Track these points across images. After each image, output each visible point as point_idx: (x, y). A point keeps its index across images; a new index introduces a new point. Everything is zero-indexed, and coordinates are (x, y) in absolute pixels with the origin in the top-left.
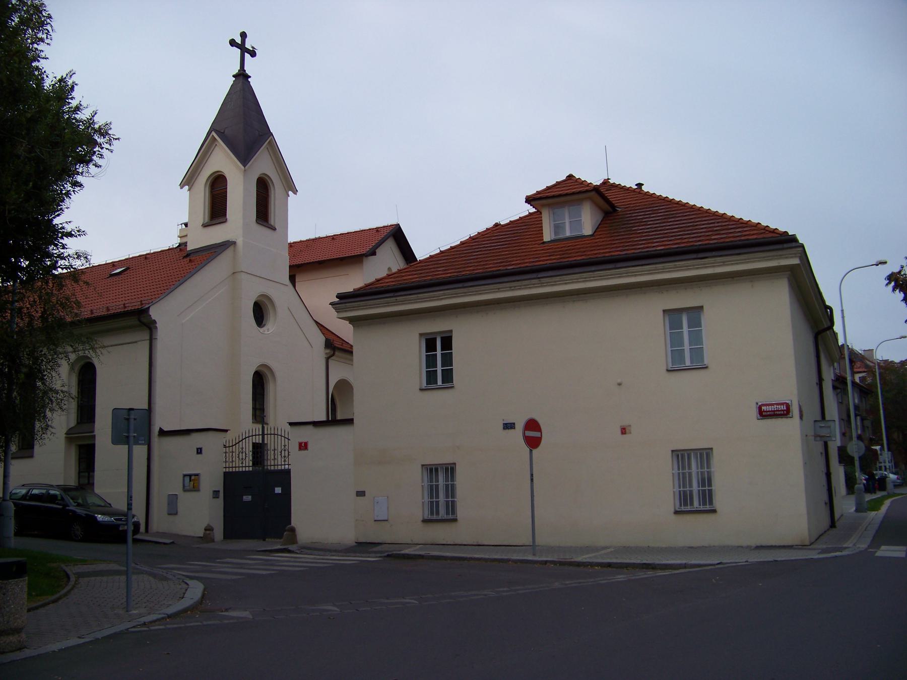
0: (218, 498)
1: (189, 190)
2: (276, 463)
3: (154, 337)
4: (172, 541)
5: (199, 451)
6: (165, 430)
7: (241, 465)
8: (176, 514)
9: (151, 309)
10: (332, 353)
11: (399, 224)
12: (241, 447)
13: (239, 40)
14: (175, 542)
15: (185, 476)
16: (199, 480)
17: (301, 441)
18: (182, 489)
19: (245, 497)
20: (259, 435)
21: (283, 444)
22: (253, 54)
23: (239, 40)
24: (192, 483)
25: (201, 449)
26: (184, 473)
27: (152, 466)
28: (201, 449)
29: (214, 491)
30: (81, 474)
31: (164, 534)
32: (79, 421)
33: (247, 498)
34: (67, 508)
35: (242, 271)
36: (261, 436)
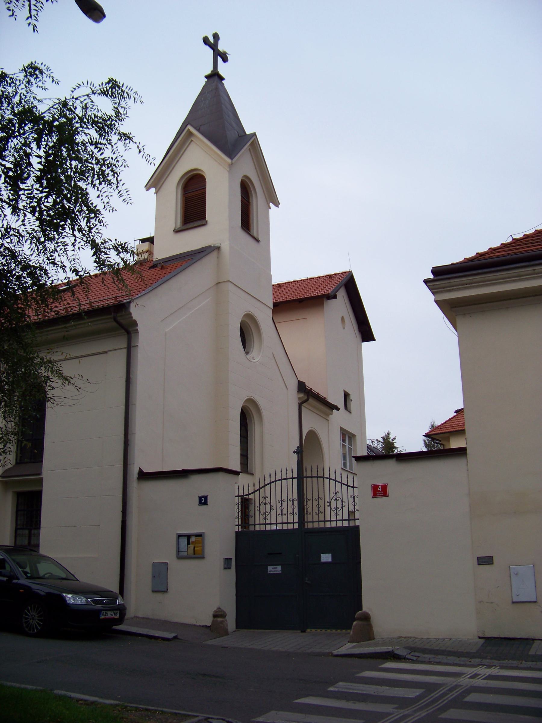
0: (230, 568)
1: (156, 192)
2: (322, 519)
3: (133, 344)
4: (173, 635)
5: (203, 501)
6: (145, 472)
7: (334, 518)
8: (166, 591)
9: (132, 305)
10: (306, 398)
11: (351, 271)
12: (262, 494)
13: (212, 40)
14: (178, 637)
15: (180, 536)
16: (203, 543)
17: (376, 483)
18: (175, 556)
19: (270, 568)
20: (306, 477)
21: (333, 490)
22: (225, 60)
23: (212, 40)
24: (192, 546)
25: (206, 498)
26: (178, 532)
27: (128, 523)
28: (206, 498)
29: (226, 559)
30: (19, 532)
31: (147, 621)
32: (18, 461)
33: (275, 569)
34: (15, 581)
35: (229, 281)
36: (295, 481)
